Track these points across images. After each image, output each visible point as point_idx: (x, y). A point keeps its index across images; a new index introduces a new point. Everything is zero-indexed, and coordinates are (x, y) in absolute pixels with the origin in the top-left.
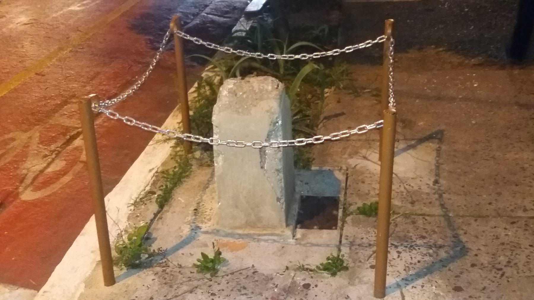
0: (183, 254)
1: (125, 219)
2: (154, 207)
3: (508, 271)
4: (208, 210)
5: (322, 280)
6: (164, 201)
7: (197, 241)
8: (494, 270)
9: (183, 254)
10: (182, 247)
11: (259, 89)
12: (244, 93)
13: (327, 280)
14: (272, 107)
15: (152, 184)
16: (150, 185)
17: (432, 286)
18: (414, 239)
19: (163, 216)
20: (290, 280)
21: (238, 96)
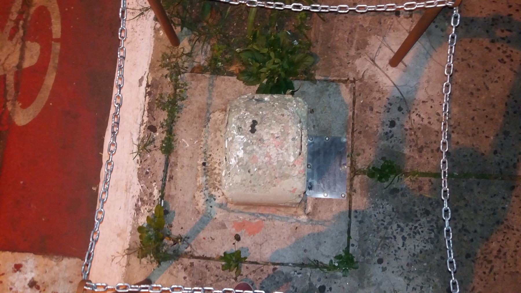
0: (204, 238)
1: (136, 180)
2: (160, 157)
3: (498, 264)
4: (216, 165)
5: (336, 280)
6: (168, 148)
7: (215, 221)
8: (485, 262)
9: (204, 238)
10: (202, 229)
11: (278, 161)
12: (259, 169)
13: (339, 281)
14: (296, 189)
15: (148, 110)
16: (146, 113)
17: (429, 287)
18: (419, 216)
19: (173, 174)
20: (307, 282)
21: (252, 173)
